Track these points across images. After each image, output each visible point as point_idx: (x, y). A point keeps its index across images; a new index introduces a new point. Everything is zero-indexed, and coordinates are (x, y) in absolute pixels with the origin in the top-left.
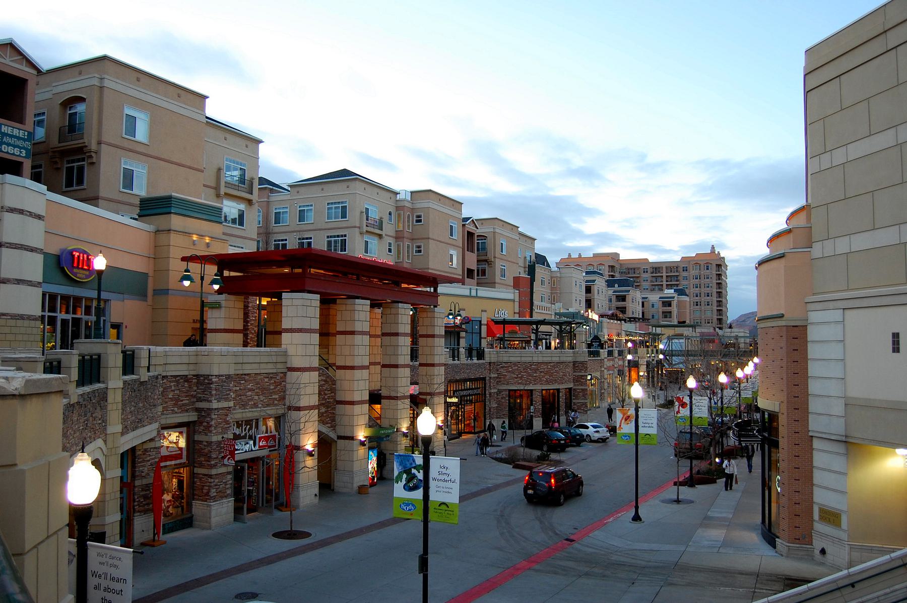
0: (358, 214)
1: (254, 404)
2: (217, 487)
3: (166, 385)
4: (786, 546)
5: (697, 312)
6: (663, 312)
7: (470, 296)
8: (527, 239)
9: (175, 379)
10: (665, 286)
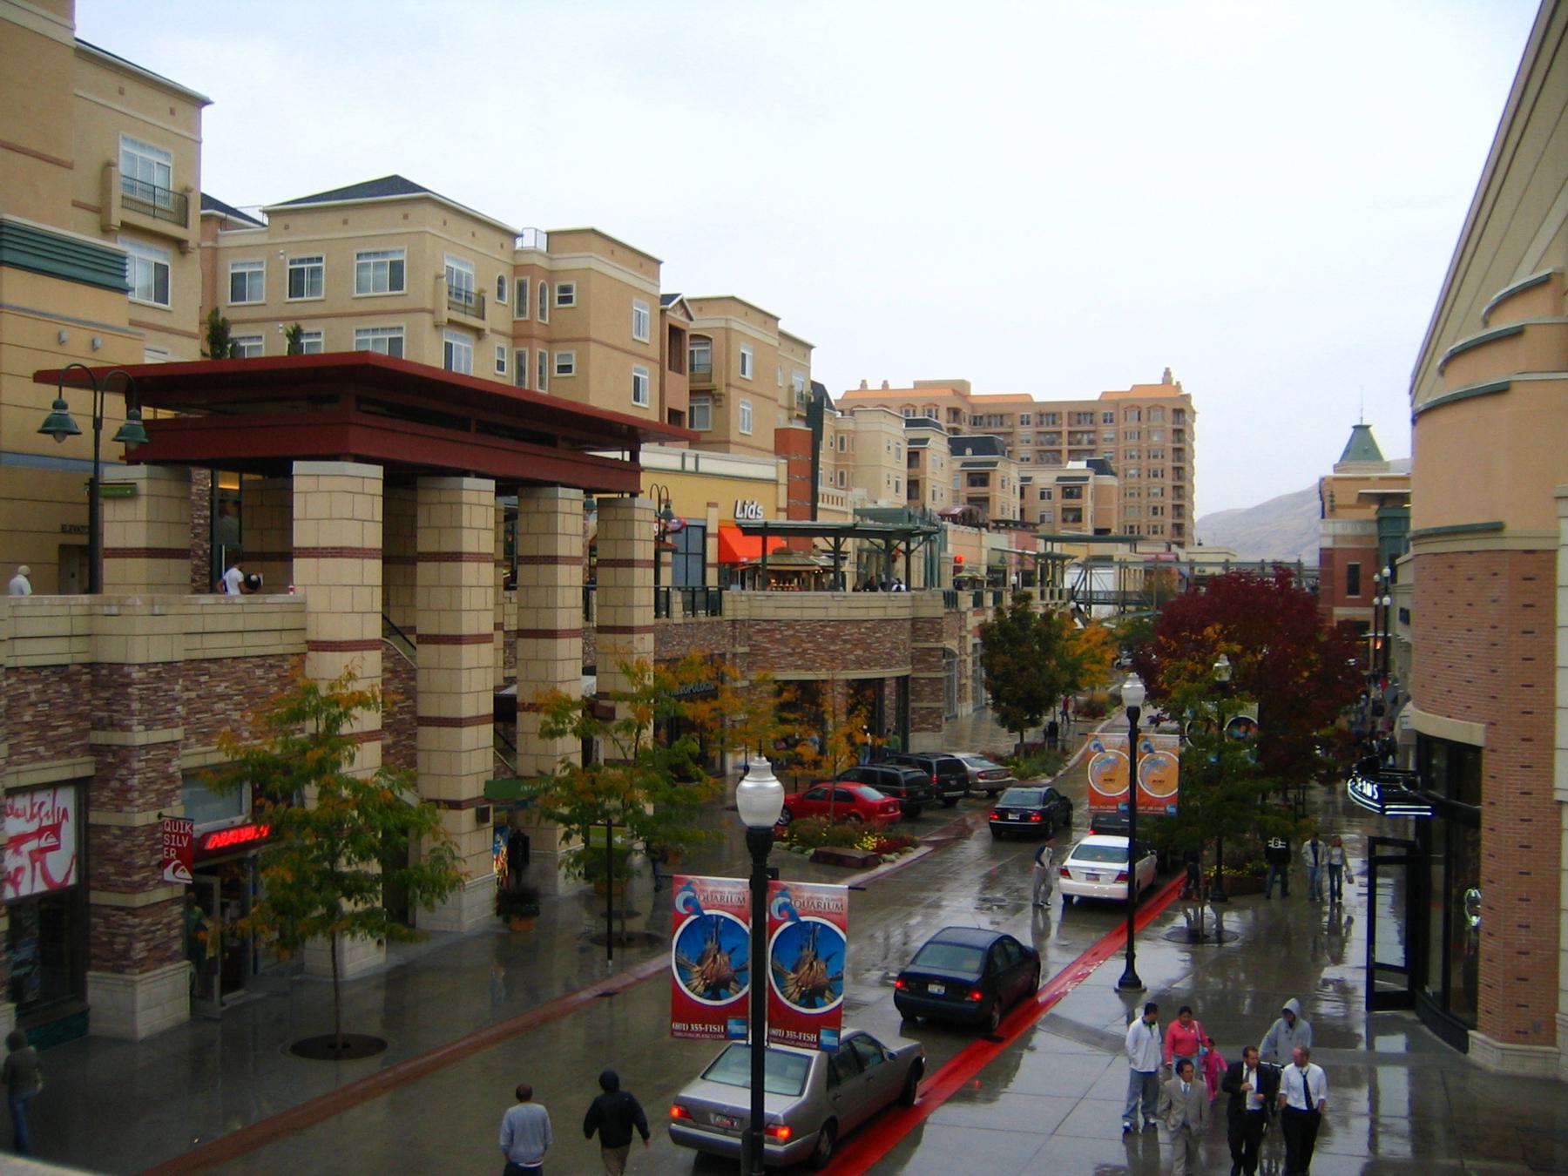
0: (429, 281)
1: (233, 731)
2: (149, 936)
3: (16, 689)
4: (1498, 1048)
7: (682, 472)
8: (794, 346)
9: (36, 676)
10: (1065, 454)
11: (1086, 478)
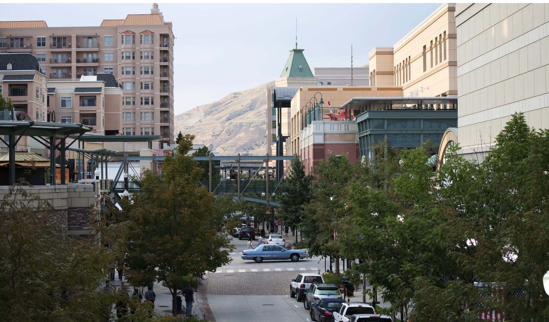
5: (128, 115)
6: (80, 114)
11: (99, 89)
